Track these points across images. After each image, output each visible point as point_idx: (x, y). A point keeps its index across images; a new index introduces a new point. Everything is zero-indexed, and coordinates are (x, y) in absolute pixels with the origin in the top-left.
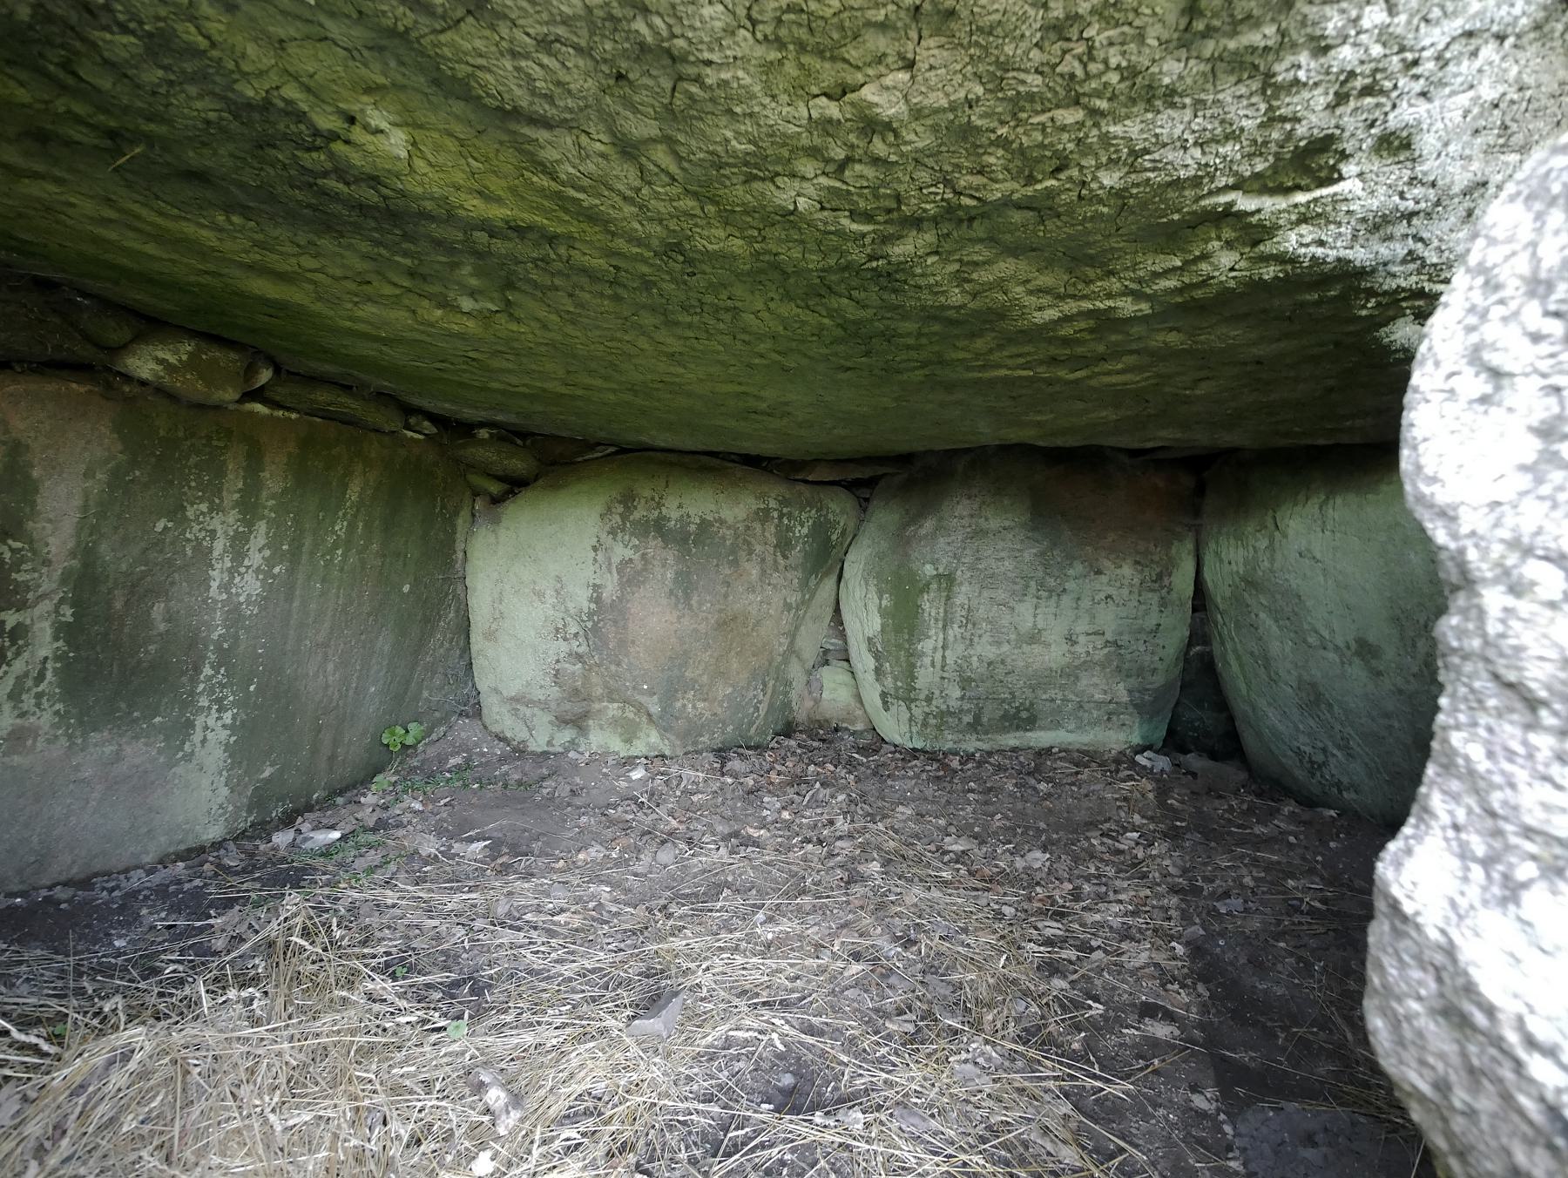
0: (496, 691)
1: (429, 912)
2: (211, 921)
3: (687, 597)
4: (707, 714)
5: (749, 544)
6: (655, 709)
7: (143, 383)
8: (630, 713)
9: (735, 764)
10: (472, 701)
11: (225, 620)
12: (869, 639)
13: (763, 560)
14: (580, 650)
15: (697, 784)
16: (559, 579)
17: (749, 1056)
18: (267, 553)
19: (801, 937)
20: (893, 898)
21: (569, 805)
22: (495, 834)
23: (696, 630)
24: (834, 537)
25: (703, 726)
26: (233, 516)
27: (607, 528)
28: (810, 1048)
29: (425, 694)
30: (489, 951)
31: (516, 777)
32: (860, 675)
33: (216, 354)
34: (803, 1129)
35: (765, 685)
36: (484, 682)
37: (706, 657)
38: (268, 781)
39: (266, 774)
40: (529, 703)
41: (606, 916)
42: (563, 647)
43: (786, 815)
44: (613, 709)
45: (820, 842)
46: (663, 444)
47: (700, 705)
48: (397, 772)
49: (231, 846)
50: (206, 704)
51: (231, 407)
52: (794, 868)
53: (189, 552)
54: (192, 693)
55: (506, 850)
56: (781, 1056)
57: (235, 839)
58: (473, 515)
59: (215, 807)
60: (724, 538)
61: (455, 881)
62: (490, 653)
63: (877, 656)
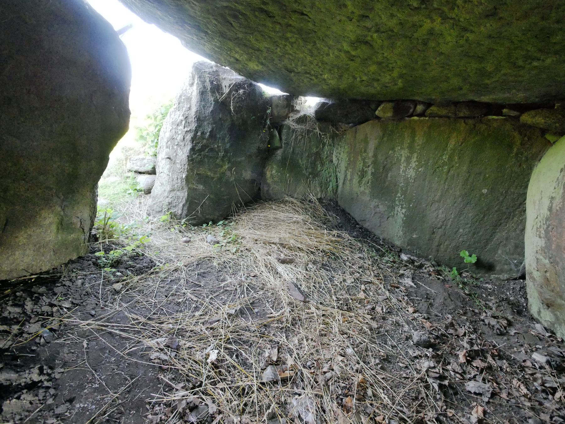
26: (406, 151)
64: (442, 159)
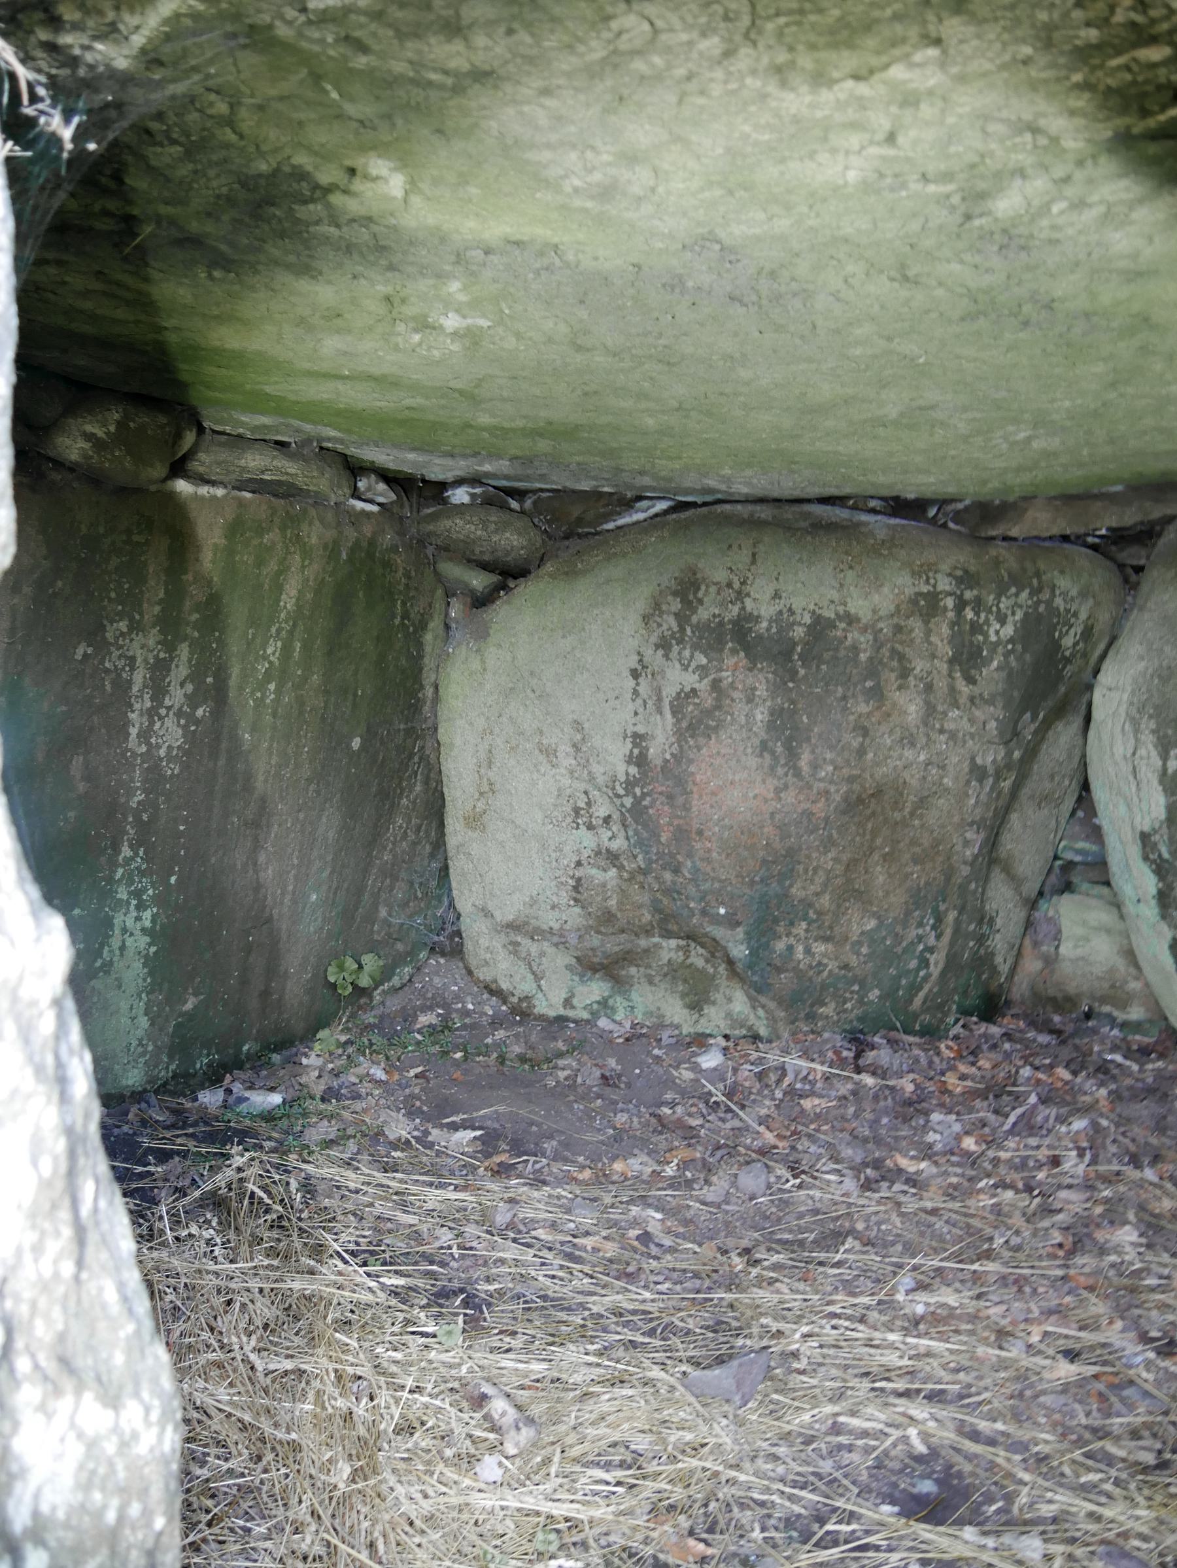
0: (487, 913)
1: (404, 1206)
2: (152, 1169)
3: (792, 755)
4: (832, 965)
5: (902, 657)
6: (740, 952)
7: (72, 468)
8: (698, 957)
9: (882, 1055)
10: (449, 929)
11: (144, 782)
12: (1145, 837)
13: (929, 688)
14: (615, 845)
15: (813, 1083)
16: (578, 726)
17: (868, 1450)
18: (189, 688)
19: (974, 1318)
20: (1151, 1281)
21: (599, 1096)
22: (489, 1123)
23: (809, 814)
24: (1068, 641)
25: (824, 987)
26: (152, 638)
27: (654, 639)
28: (970, 1458)
29: (383, 912)
30: (485, 1264)
31: (517, 1049)
32: (1130, 908)
33: (142, 418)
34: (944, 1542)
35: (939, 919)
36: (466, 898)
37: (827, 861)
38: (190, 1016)
39: (189, 1006)
40: (536, 934)
41: (654, 1250)
42: (587, 840)
43: (969, 1143)
44: (669, 949)
45: (1029, 1189)
46: (745, 490)
47: (819, 948)
48: (347, 1030)
49: (153, 1099)
50: (125, 897)
51: (153, 488)
52: (976, 1223)
53: (108, 687)
54: (110, 880)
55: (504, 1146)
56: (919, 1459)
57: (156, 1092)
58: (447, 627)
59: (135, 1043)
60: (855, 648)
61: (437, 1175)
62: (475, 850)
63: (1160, 869)
64: (265, 657)
